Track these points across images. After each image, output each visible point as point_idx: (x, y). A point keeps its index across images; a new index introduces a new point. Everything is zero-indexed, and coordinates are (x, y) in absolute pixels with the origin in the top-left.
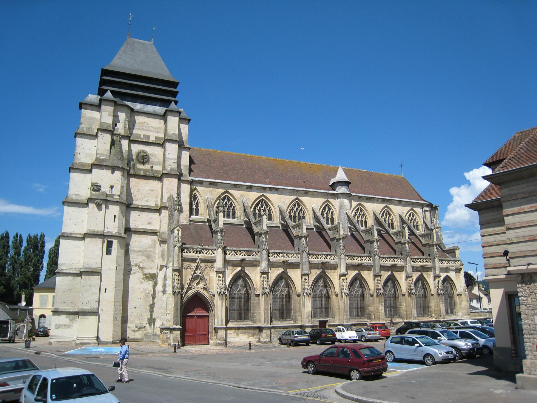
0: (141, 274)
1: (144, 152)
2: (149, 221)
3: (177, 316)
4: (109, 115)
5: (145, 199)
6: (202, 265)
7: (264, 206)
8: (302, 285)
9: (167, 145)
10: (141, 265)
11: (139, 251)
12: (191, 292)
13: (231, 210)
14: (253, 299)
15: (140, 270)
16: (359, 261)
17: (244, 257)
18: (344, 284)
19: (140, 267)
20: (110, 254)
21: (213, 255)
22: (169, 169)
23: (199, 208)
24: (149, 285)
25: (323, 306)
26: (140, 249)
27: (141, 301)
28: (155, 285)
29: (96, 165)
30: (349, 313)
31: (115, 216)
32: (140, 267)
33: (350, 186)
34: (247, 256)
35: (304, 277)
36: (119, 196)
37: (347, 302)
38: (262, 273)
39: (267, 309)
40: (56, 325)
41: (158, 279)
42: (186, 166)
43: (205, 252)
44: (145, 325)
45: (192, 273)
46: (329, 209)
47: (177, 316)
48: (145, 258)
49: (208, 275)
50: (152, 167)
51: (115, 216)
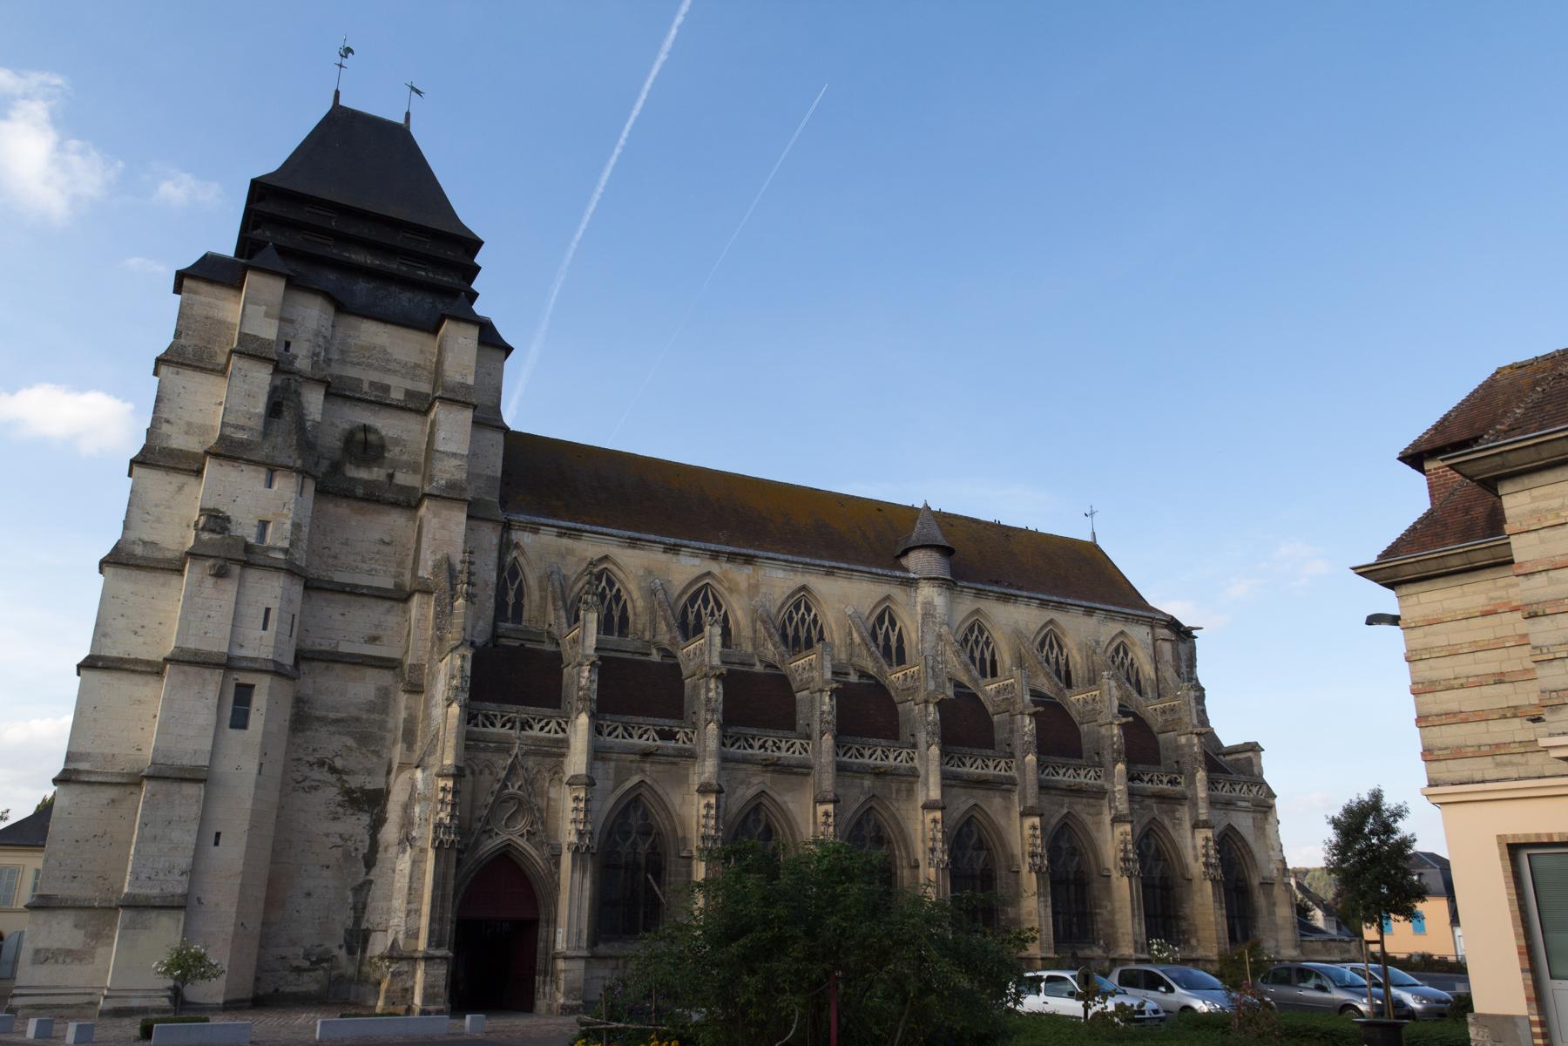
0: (335, 790)
1: (366, 429)
2: (374, 632)
3: (441, 920)
4: (267, 315)
5: (365, 567)
6: (530, 762)
7: (712, 603)
10: (339, 763)
12: (491, 845)
13: (616, 614)
15: (333, 778)
19: (333, 770)
20: (244, 726)
21: (561, 735)
23: (526, 601)
27: (327, 873)
28: (378, 823)
32: (333, 770)
34: (659, 743)
40: (37, 952)
45: (497, 786)
46: (893, 623)
47: (441, 920)
48: (350, 742)
50: (391, 476)
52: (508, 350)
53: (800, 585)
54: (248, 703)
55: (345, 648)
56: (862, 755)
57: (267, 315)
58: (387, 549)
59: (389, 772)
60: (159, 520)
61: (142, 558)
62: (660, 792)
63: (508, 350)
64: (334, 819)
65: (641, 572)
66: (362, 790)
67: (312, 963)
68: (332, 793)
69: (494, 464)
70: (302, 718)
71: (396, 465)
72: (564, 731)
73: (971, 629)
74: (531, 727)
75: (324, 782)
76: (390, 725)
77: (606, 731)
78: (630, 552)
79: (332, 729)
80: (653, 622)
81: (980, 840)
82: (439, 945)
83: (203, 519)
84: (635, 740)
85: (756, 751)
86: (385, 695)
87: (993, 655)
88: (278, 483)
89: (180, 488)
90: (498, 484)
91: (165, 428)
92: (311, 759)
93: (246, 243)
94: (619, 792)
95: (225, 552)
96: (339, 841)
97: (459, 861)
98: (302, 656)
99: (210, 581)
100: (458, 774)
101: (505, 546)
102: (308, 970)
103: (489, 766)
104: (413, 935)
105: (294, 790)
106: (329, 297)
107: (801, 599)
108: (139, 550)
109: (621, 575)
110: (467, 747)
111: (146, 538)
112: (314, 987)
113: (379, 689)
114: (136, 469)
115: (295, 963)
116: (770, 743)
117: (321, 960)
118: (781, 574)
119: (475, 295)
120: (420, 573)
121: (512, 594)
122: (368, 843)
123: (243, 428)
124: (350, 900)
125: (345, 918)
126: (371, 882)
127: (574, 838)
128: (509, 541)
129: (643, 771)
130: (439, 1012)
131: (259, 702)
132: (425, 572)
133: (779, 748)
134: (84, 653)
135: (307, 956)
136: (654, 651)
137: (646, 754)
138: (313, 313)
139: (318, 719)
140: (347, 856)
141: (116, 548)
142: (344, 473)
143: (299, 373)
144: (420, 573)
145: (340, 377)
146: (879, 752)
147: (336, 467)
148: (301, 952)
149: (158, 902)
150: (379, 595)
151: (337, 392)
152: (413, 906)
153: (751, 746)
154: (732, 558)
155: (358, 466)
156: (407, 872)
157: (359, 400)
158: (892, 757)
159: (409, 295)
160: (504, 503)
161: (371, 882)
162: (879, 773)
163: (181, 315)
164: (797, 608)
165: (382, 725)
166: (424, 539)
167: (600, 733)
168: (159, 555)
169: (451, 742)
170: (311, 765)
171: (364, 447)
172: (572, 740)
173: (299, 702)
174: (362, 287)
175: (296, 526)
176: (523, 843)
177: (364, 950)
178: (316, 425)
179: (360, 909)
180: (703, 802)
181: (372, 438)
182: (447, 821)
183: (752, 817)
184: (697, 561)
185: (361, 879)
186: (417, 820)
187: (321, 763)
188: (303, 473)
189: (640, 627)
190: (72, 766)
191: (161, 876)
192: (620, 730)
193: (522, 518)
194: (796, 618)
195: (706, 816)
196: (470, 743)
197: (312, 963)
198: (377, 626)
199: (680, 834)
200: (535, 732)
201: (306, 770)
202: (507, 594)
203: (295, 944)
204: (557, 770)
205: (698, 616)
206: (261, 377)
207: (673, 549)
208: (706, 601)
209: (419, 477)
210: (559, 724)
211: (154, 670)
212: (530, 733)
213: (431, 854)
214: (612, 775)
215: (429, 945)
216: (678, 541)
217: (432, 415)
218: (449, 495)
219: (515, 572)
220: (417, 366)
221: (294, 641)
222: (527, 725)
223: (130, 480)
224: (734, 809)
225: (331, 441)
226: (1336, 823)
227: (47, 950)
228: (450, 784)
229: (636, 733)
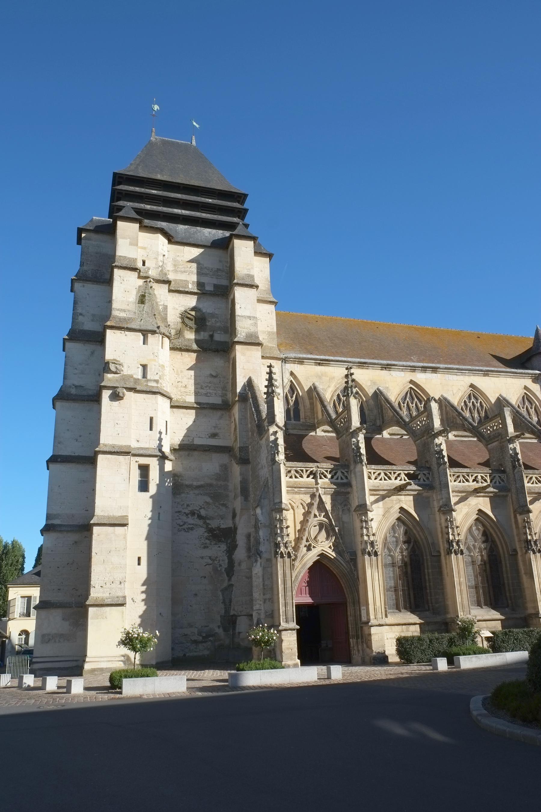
0: (203, 530)
2: (213, 431)
10: (203, 513)
15: (200, 522)
17: (403, 482)
19: (200, 517)
21: (345, 481)
22: (244, 334)
24: (218, 550)
26: (199, 483)
28: (232, 548)
31: (139, 559)
32: (200, 517)
42: (272, 333)
48: (208, 499)
50: (212, 336)
51: (139, 559)
58: (215, 380)
59: (234, 516)
61: (76, 395)
64: (205, 547)
66: (219, 528)
67: (203, 637)
68: (201, 531)
72: (347, 478)
75: (196, 525)
76: (231, 487)
77: (373, 477)
79: (197, 492)
86: (225, 468)
91: (80, 318)
92: (187, 511)
96: (211, 562)
102: (202, 642)
105: (179, 531)
108: (73, 391)
111: (76, 383)
112: (206, 653)
114: (51, 466)
115: (193, 638)
116: (479, 477)
117: (209, 636)
122: (227, 561)
124: (221, 597)
126: (232, 585)
134: (49, 454)
135: (200, 634)
139: (188, 486)
140: (215, 570)
141: (60, 390)
148: (196, 631)
149: (109, 601)
152: (268, 596)
154: (424, 369)
156: (260, 574)
161: (232, 585)
168: (85, 393)
170: (187, 515)
172: (354, 483)
177: (234, 628)
179: (228, 603)
184: (402, 374)
185: (225, 584)
186: (261, 540)
187: (193, 513)
190: (50, 522)
191: (108, 584)
192: (382, 475)
197: (203, 637)
198: (215, 427)
201: (184, 518)
203: (191, 626)
220: (218, 270)
223: (79, 247)
226: (140, 617)
227: (49, 635)
229: (393, 477)
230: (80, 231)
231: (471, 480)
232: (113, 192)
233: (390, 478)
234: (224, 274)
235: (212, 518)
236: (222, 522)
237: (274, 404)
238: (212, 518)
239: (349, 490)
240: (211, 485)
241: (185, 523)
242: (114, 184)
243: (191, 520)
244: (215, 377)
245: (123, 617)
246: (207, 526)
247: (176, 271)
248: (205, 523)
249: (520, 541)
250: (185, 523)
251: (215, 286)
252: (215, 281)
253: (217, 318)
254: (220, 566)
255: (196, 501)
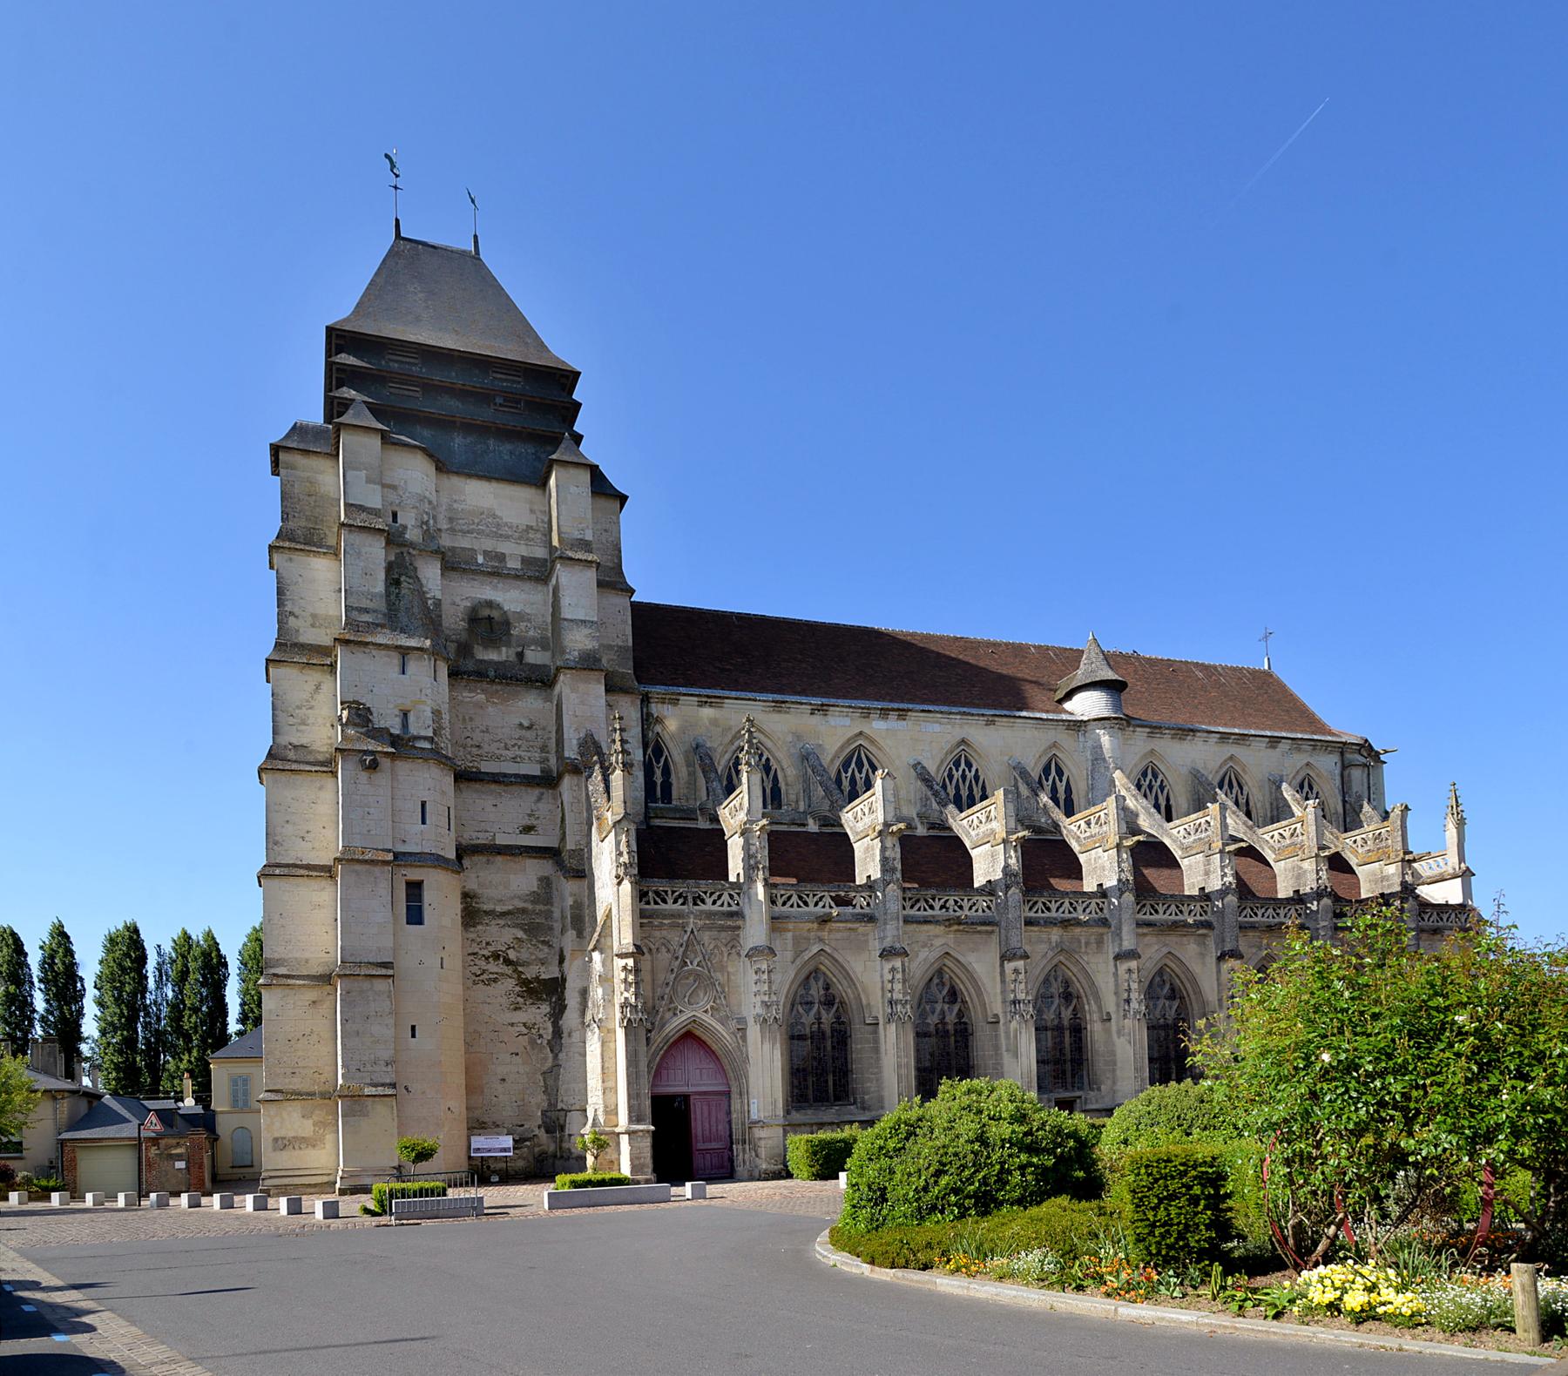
1: (490, 604)
6: (706, 937)
8: (1003, 992)
9: (564, 576)
10: (512, 955)
11: (503, 914)
12: (675, 1024)
14: (859, 1034)
15: (508, 970)
16: (1173, 917)
17: (827, 909)
18: (1134, 986)
19: (508, 962)
20: (420, 922)
21: (734, 908)
23: (673, 779)
24: (538, 1013)
25: (1067, 1064)
26: (505, 908)
27: (518, 1059)
29: (347, 642)
30: (1147, 1074)
32: (508, 962)
33: (1124, 695)
35: (1009, 966)
36: (431, 740)
37: (1141, 1040)
38: (887, 954)
39: (907, 1065)
40: (276, 1140)
41: (568, 994)
42: (625, 649)
43: (709, 901)
44: (540, 805)
46: (1060, 773)
47: (638, 1095)
48: (520, 934)
49: (723, 969)
50: (520, 655)
52: (623, 499)
53: (958, 739)
54: (419, 898)
55: (501, 840)
56: (1049, 909)
57: (369, 481)
58: (528, 734)
59: (562, 960)
60: (304, 723)
62: (840, 960)
63: (623, 499)
64: (516, 1009)
65: (790, 738)
68: (510, 984)
69: (623, 632)
70: (472, 913)
71: (524, 643)
73: (1145, 774)
74: (703, 901)
76: (557, 914)
77: (780, 901)
78: (776, 717)
79: (502, 922)
80: (807, 791)
81: (1173, 989)
82: (639, 1120)
83: (345, 713)
84: (811, 908)
85: (937, 912)
86: (546, 882)
87: (1168, 799)
88: (412, 666)
89: (318, 687)
90: (630, 655)
92: (486, 952)
93: (335, 408)
94: (799, 962)
95: (378, 744)
96: (525, 1031)
97: (648, 1039)
98: (463, 851)
99: (364, 776)
100: (638, 952)
101: (647, 720)
103: (666, 943)
104: (611, 1111)
105: (475, 983)
106: (428, 454)
107: (961, 758)
109: (769, 744)
110: (642, 925)
113: (541, 879)
118: (937, 727)
119: (578, 439)
120: (566, 754)
121: (658, 772)
123: (366, 611)
125: (538, 1101)
127: (759, 1010)
128: (649, 715)
129: (821, 940)
130: (647, 1181)
131: (428, 896)
132: (571, 752)
133: (961, 907)
136: (811, 821)
137: (825, 920)
138: (414, 473)
140: (532, 1042)
142: (479, 654)
143: (412, 545)
144: (566, 754)
145: (453, 549)
146: (1067, 904)
147: (464, 649)
150: (528, 781)
151: (453, 564)
153: (932, 907)
155: (486, 647)
156: (599, 1051)
157: (474, 572)
158: (1080, 909)
159: (509, 447)
160: (638, 667)
162: (1066, 924)
163: (285, 497)
164: (957, 764)
165: (548, 915)
166: (565, 717)
167: (773, 903)
169: (627, 919)
171: (488, 625)
172: (747, 912)
173: (466, 896)
174: (458, 442)
175: (437, 713)
176: (708, 1019)
178: (438, 603)
179: (551, 1091)
180: (888, 966)
181: (495, 614)
182: (633, 1000)
183: (936, 981)
184: (847, 721)
185: (549, 1063)
187: (496, 956)
188: (435, 653)
189: (793, 797)
192: (795, 899)
193: (660, 689)
194: (957, 775)
195: (891, 981)
196: (644, 918)
199: (864, 1002)
200: (708, 906)
201: (482, 963)
202: (653, 773)
204: (733, 944)
205: (853, 781)
206: (376, 553)
207: (822, 709)
208: (860, 765)
209: (548, 654)
210: (731, 896)
211: (327, 871)
212: (702, 907)
213: (620, 1035)
214: (790, 946)
215: (631, 1121)
216: (825, 701)
217: (554, 581)
218: (588, 663)
219: (658, 751)
220: (529, 528)
221: (453, 834)
222: (698, 900)
224: (918, 974)
225: (454, 620)
228: (630, 962)
230: (276, 450)
231: (937, 907)
232: (330, 366)
233: (806, 904)
234: (539, 535)
235: (525, 964)
236: (543, 969)
237: (740, 616)
238: (525, 964)
239: (740, 923)
240: (524, 911)
241: (484, 972)
242: (329, 354)
243: (494, 967)
244: (530, 728)
245: (767, 768)
246: (519, 978)
247: (452, 531)
248: (515, 971)
249: (1004, 1002)
250: (484, 972)
251: (524, 560)
252: (524, 551)
253: (529, 620)
254: (541, 1036)
255: (501, 935)
